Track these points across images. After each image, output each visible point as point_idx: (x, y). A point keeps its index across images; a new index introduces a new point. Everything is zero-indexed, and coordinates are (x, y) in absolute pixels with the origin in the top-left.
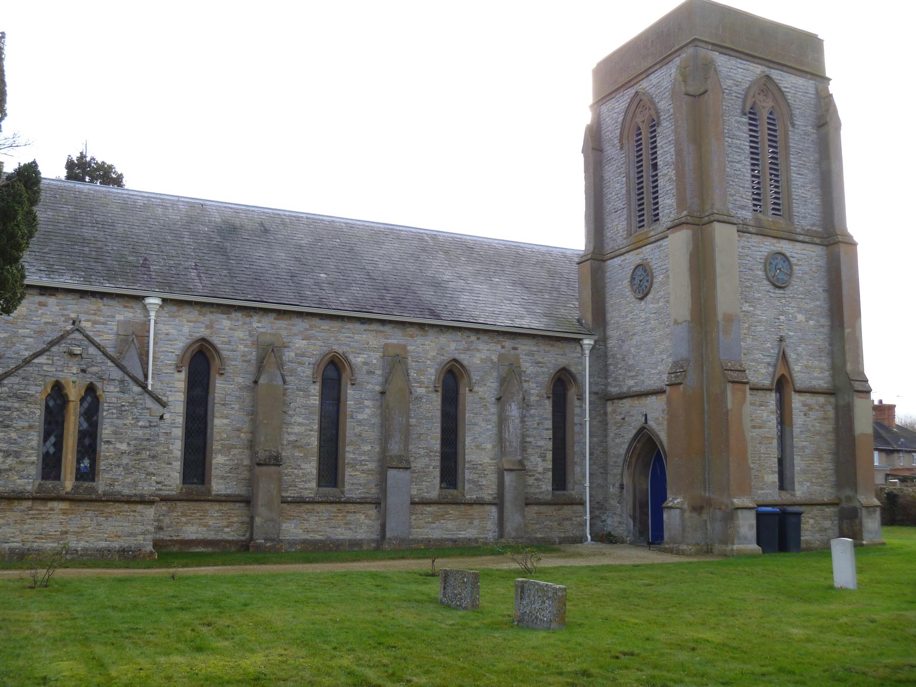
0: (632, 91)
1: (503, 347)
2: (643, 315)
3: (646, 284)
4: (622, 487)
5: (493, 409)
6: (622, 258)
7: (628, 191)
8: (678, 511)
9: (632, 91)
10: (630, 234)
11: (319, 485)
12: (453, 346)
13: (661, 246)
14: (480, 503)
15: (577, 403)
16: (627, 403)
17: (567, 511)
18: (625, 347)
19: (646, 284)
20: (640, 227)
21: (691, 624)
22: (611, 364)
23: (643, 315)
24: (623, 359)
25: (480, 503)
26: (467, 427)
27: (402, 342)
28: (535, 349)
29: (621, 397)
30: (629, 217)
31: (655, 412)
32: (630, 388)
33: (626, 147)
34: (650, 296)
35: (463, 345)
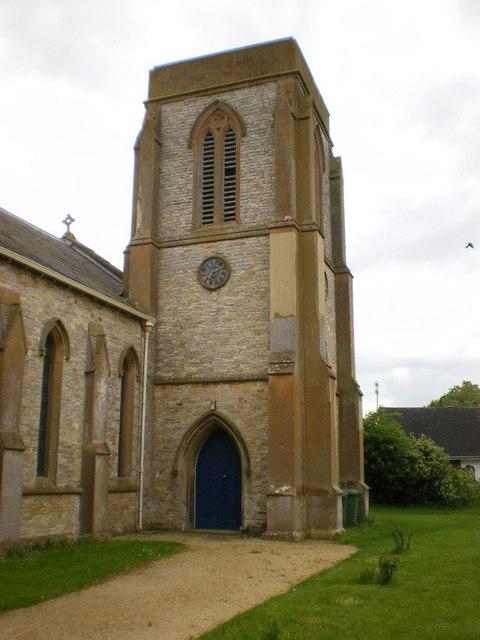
0: (209, 100)
1: (92, 316)
2: (214, 305)
3: (222, 276)
4: (175, 474)
5: (82, 383)
6: (186, 248)
7: (195, 187)
8: (288, 499)
9: (209, 100)
10: (194, 228)
11: (46, 476)
12: (57, 304)
13: (243, 243)
14: (68, 492)
15: (136, 385)
16: (186, 390)
17: (125, 498)
18: (185, 334)
19: (222, 276)
20: (226, 221)
21: (454, 621)
22: (162, 350)
23: (214, 305)
24: (182, 345)
25: (68, 492)
26: (63, 402)
27: (16, 290)
28: (113, 323)
29: (177, 383)
30: (194, 212)
31: (228, 402)
32: (190, 374)
33: (195, 147)
34: (225, 289)
35: (64, 306)
